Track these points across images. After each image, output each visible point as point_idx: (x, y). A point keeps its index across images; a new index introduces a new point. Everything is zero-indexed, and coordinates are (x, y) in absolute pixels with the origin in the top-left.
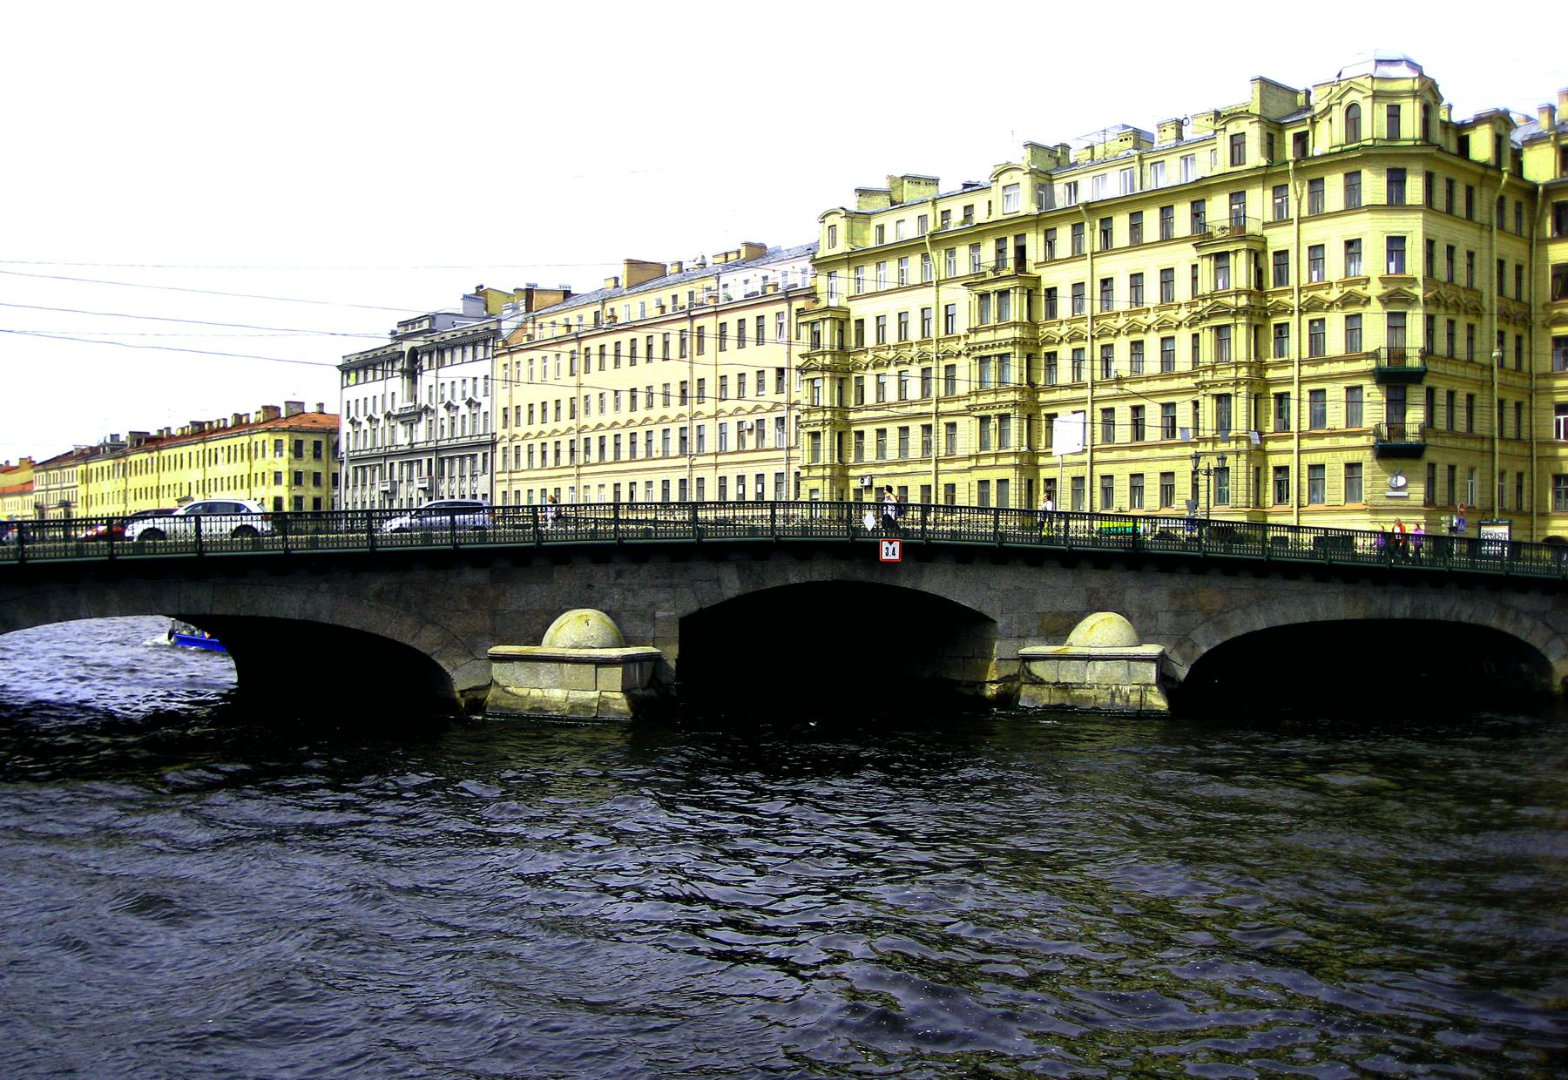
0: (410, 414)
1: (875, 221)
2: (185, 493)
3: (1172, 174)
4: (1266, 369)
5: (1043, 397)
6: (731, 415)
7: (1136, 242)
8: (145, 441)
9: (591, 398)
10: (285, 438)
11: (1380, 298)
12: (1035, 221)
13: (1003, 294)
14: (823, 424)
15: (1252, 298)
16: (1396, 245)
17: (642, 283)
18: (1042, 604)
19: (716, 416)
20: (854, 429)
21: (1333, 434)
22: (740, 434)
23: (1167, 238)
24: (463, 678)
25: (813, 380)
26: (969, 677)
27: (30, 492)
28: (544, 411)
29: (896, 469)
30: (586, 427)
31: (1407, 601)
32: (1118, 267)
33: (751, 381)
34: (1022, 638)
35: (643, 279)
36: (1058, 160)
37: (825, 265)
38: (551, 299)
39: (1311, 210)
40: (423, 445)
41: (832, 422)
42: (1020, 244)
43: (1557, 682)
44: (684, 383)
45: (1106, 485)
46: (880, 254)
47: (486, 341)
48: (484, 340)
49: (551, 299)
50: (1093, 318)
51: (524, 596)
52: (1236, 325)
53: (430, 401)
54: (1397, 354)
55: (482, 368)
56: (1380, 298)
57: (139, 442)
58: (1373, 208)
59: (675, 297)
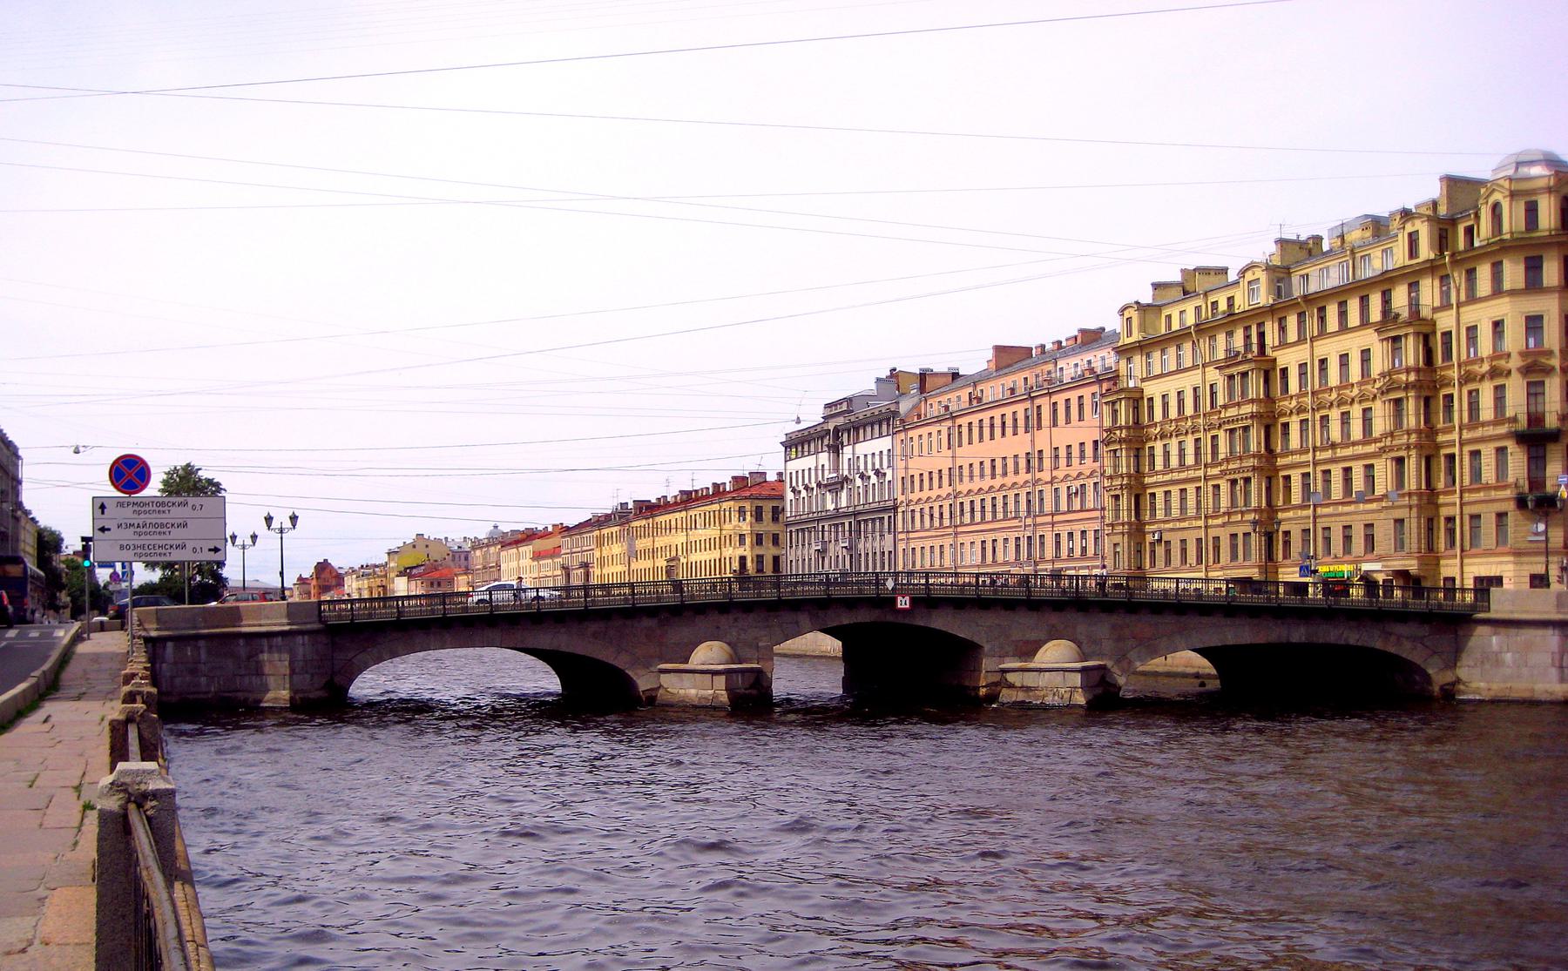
0: (833, 484)
1: (1165, 312)
2: (674, 554)
3: (1376, 264)
4: (1437, 434)
5: (1147, 480)
6: (1062, 481)
7: (1344, 328)
8: (647, 509)
9: (974, 466)
10: (747, 505)
11: (1519, 370)
12: (1271, 311)
13: (1244, 375)
14: (1121, 488)
15: (1421, 374)
16: (1534, 324)
17: (1009, 366)
18: (1016, 635)
19: (1051, 482)
20: (1149, 491)
21: (1488, 488)
22: (1069, 496)
23: (1497, 291)
24: (644, 683)
25: (1115, 451)
26: (973, 684)
27: (559, 555)
28: (931, 479)
29: (1178, 525)
30: (960, 492)
31: (1302, 630)
32: (1330, 349)
33: (1075, 452)
34: (1002, 656)
35: (1010, 362)
36: (1310, 252)
37: (1125, 352)
38: (942, 380)
39: (1467, 297)
40: (845, 510)
41: (1129, 487)
42: (1262, 330)
43: (1437, 689)
44: (1028, 454)
45: (1326, 535)
46: (1162, 342)
47: (888, 420)
48: (885, 421)
49: (942, 380)
50: (1313, 393)
51: (678, 633)
52: (1407, 398)
53: (850, 472)
54: (1535, 419)
55: (884, 444)
56: (1519, 370)
57: (641, 509)
58: (1513, 293)
59: (1026, 379)
